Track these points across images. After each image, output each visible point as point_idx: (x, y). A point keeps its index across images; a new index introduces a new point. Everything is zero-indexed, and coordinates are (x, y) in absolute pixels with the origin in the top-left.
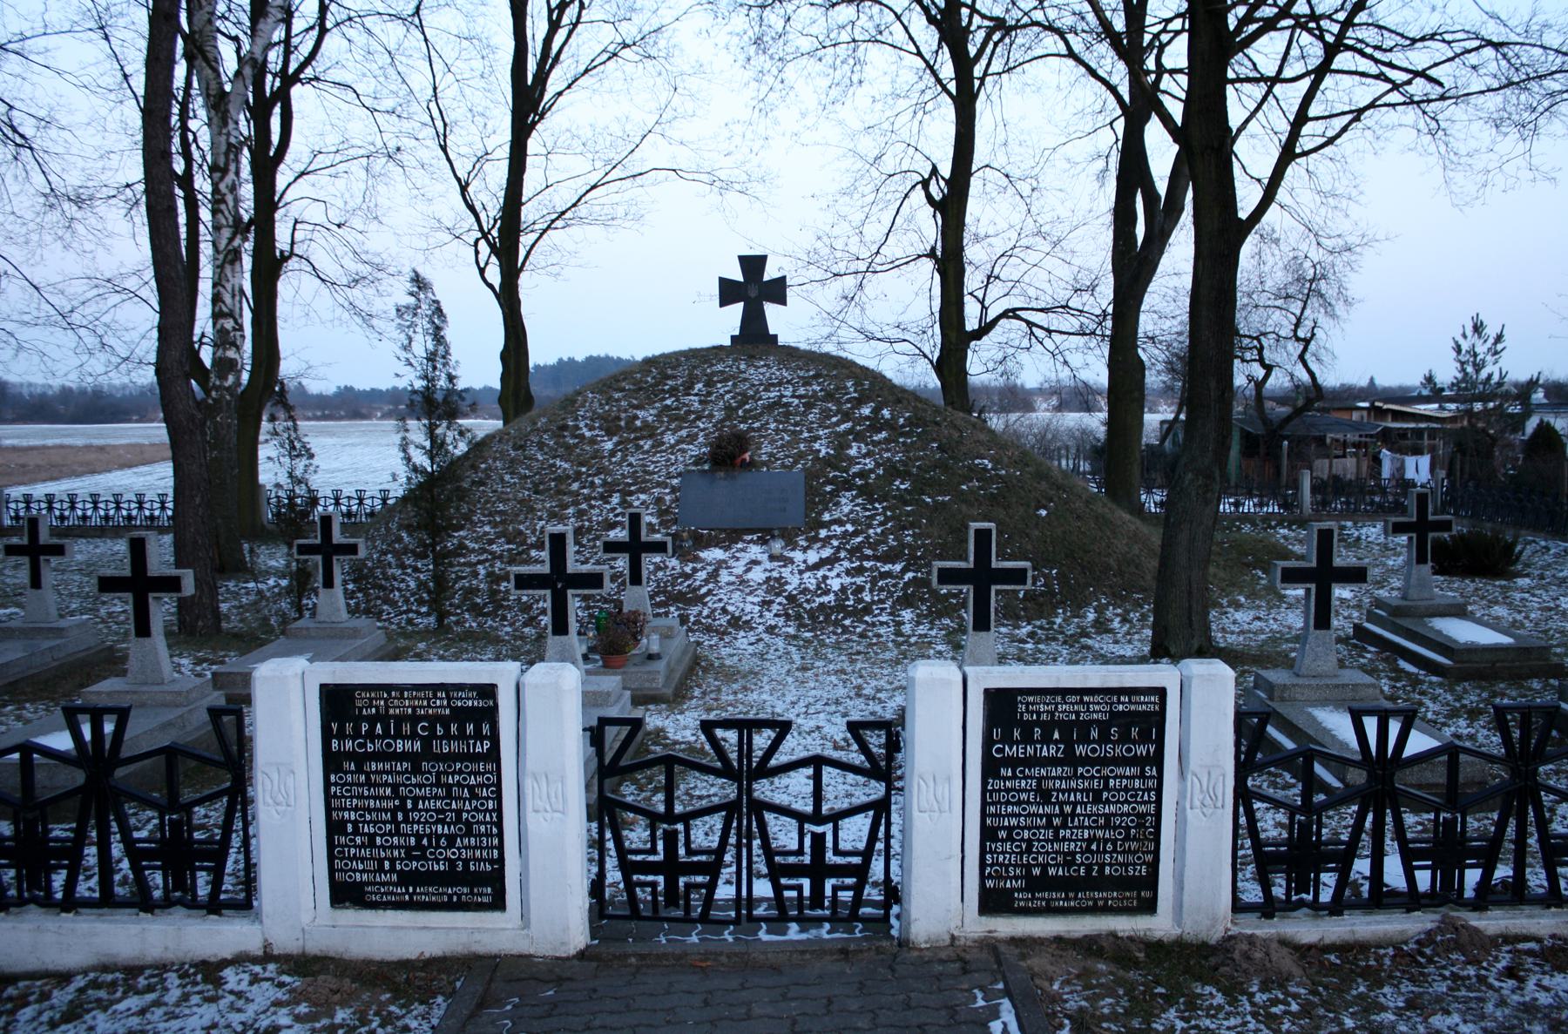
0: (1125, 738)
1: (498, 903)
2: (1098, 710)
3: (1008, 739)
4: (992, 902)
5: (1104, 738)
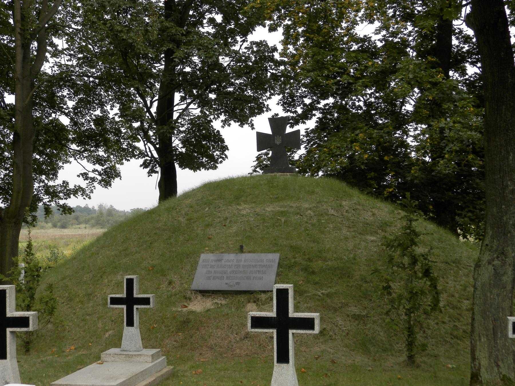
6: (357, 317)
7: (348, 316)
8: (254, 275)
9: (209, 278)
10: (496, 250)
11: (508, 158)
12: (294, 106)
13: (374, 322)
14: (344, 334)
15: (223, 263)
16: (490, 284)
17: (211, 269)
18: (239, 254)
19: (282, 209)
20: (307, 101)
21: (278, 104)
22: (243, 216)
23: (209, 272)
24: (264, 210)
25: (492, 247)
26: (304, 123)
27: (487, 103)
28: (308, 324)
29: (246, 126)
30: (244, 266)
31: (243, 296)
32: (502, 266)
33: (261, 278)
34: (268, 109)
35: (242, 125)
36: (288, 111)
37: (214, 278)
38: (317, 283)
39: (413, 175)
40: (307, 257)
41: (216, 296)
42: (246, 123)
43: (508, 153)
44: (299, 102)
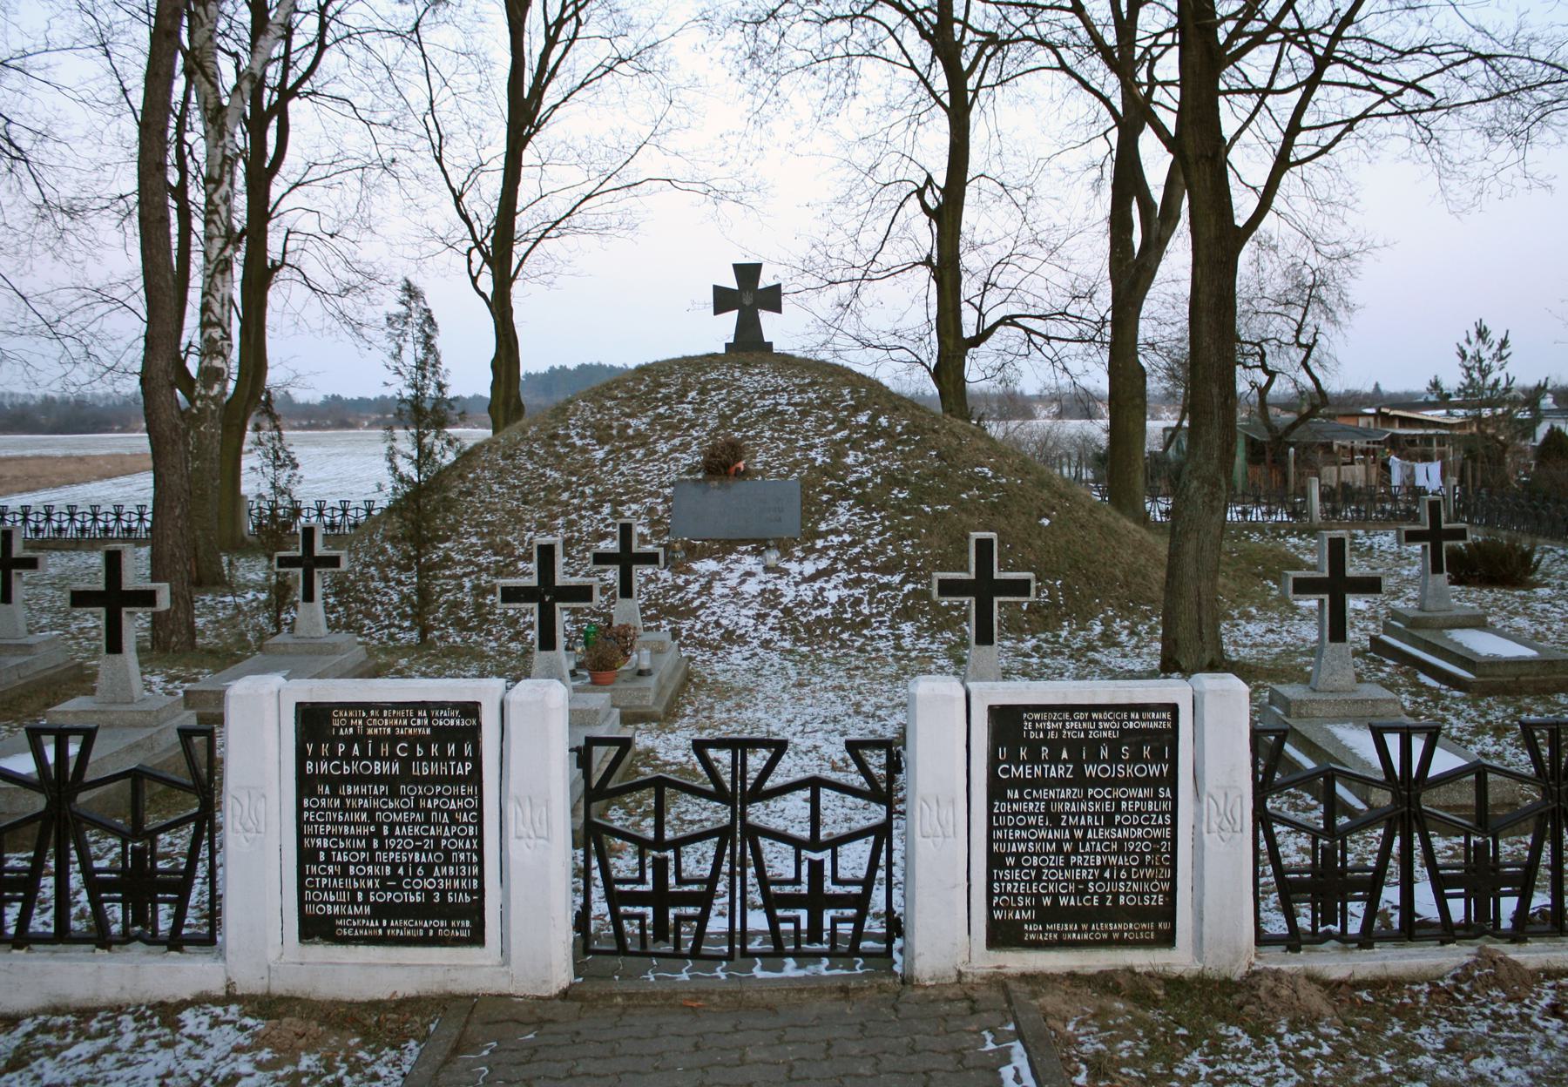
0: (1136, 758)
1: (477, 937)
2: (1107, 728)
3: (1014, 759)
4: (1002, 935)
5: (1115, 758)
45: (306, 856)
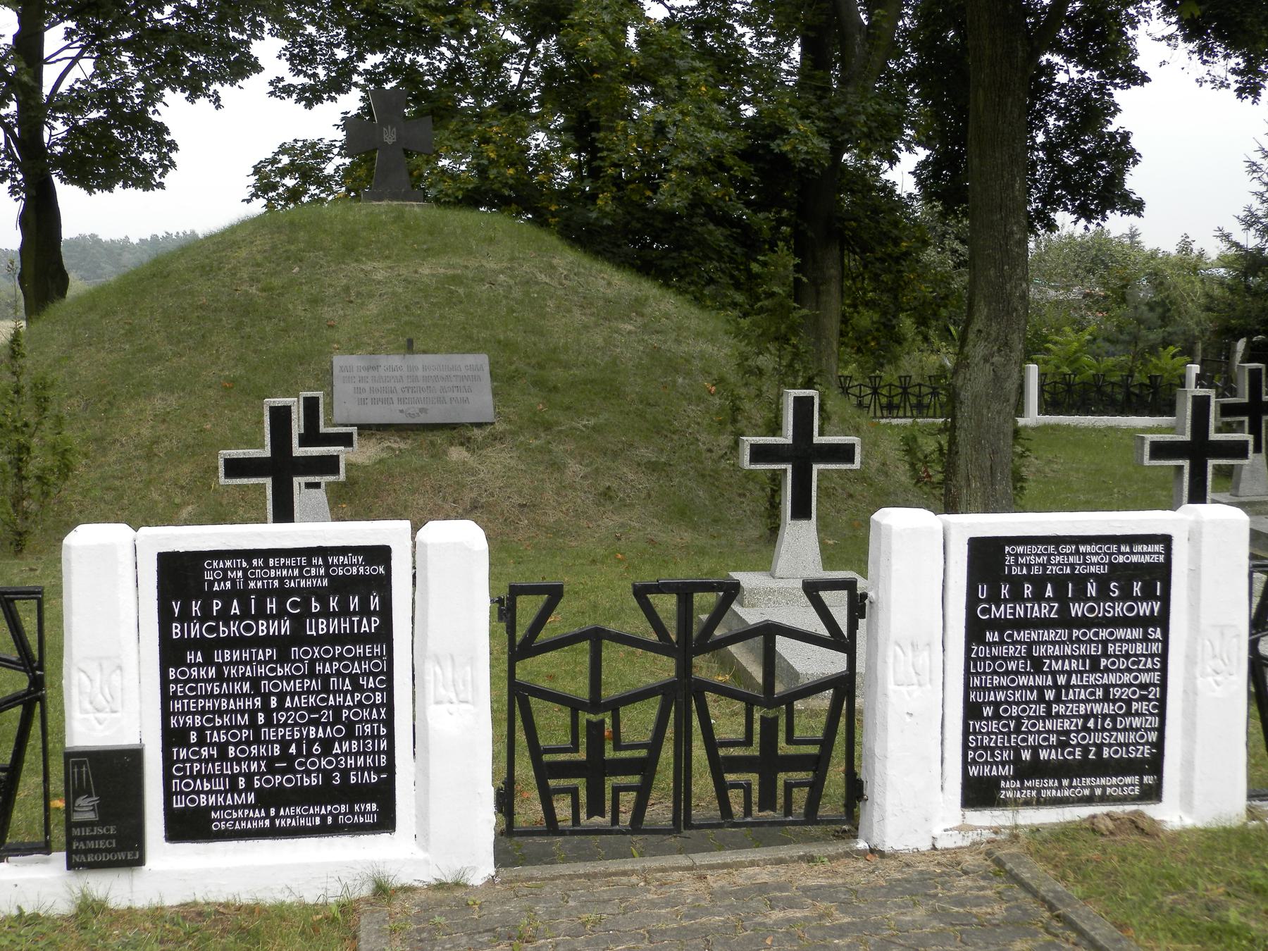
0: (1126, 595)
1: (386, 822)
2: (1096, 562)
3: (995, 598)
4: (978, 793)
5: (1103, 594)
6: (653, 467)
7: (639, 465)
8: (450, 394)
9: (363, 402)
10: (996, 339)
11: (1013, 186)
12: (312, 62)
13: (684, 474)
14: (643, 496)
15: (382, 372)
16: (987, 395)
17: (362, 385)
18: (408, 356)
19: (450, 272)
20: (341, 54)
21: (279, 57)
22: (379, 282)
23: (359, 390)
24: (416, 272)
25: (989, 334)
26: (333, 99)
27: (981, 92)
28: (844, 453)
29: (202, 102)
30: (426, 379)
31: (438, 433)
32: (1005, 366)
33: (466, 401)
34: (257, 68)
35: (192, 99)
36: (299, 73)
37: (374, 401)
38: (568, 408)
39: (600, 210)
40: (534, 361)
41: (385, 435)
42: (205, 95)
43: (1013, 178)
44: (324, 55)
45: (972, 711)
